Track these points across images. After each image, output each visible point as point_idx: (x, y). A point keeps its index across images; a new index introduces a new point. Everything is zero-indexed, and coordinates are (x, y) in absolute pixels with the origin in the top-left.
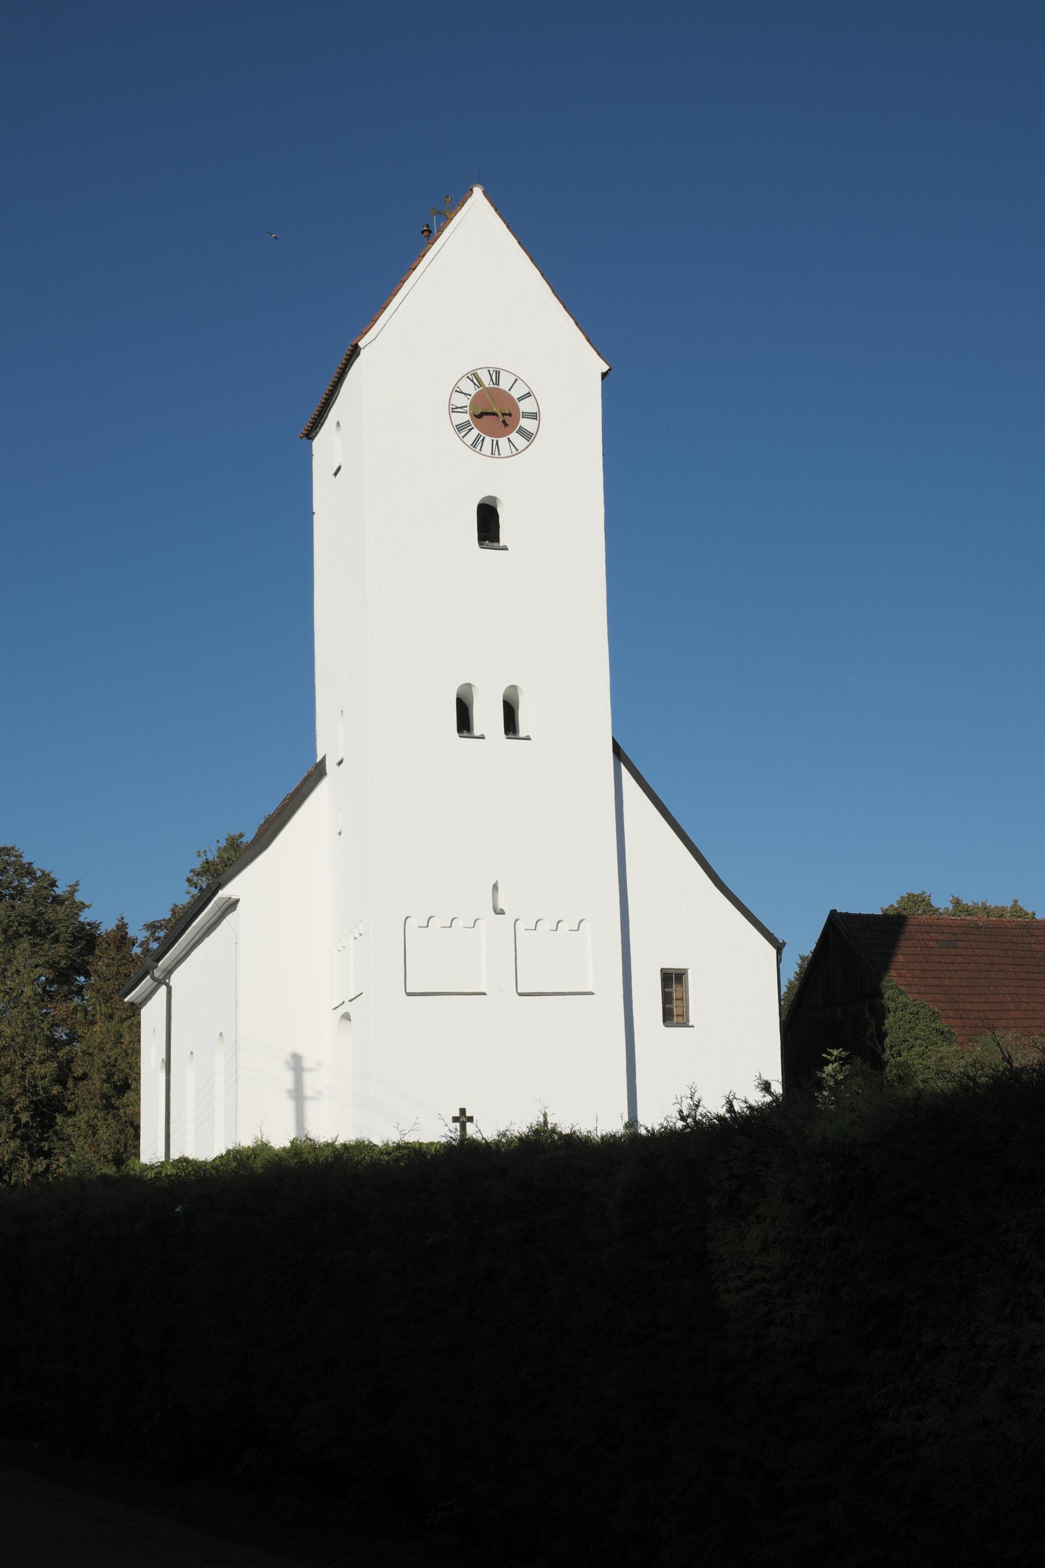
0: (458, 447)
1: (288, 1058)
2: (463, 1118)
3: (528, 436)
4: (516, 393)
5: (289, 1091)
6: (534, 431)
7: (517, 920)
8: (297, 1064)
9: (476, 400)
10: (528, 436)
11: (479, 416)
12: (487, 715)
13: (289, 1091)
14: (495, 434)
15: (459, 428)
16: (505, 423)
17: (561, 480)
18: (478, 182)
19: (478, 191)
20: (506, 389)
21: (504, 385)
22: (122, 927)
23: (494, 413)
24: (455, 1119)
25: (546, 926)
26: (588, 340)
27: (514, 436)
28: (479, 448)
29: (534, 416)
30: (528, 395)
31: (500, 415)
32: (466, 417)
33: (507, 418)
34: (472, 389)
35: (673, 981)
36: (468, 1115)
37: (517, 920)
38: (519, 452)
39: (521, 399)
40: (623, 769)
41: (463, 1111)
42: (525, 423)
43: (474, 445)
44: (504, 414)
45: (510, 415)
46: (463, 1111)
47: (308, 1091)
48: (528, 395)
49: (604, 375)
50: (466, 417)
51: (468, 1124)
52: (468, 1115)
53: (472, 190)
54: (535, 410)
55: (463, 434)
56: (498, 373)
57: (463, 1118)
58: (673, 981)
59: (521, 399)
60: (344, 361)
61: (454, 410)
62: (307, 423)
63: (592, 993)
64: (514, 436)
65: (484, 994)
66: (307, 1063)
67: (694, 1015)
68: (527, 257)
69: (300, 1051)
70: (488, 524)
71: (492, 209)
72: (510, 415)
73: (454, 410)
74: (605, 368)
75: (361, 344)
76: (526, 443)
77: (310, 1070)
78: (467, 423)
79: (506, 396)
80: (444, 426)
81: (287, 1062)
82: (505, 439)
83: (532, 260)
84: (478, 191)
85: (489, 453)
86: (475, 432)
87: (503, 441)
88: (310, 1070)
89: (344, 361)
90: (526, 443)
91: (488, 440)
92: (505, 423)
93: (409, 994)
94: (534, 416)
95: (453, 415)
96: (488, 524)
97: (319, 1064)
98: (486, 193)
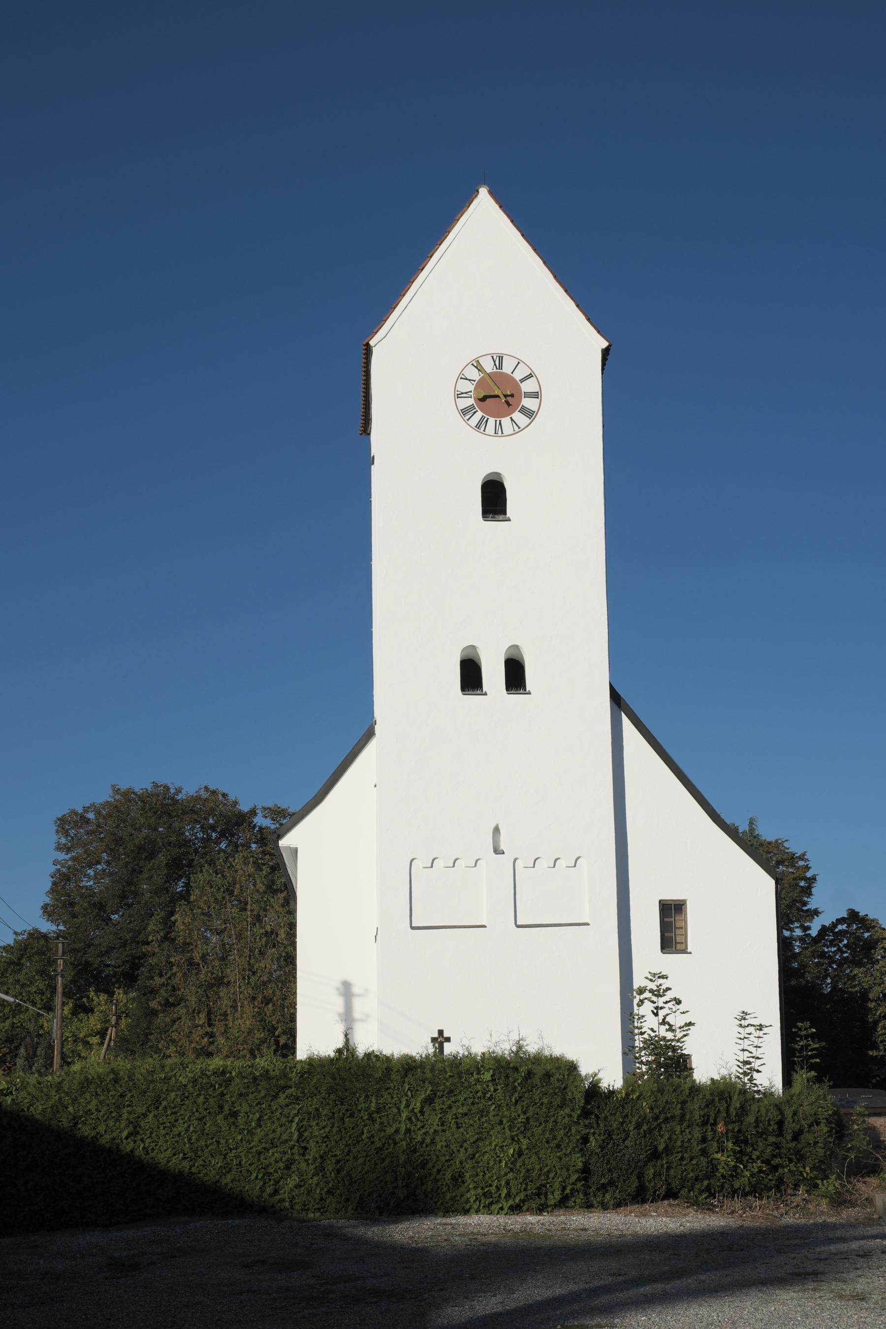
0: (464, 430)
1: (339, 985)
2: (440, 1039)
3: (530, 414)
4: (518, 376)
5: (340, 1015)
6: (535, 409)
7: (515, 860)
8: (347, 991)
9: (480, 384)
10: (530, 414)
11: (483, 399)
12: (493, 674)
13: (340, 1015)
14: (498, 414)
15: (464, 412)
16: (508, 404)
17: (563, 455)
18: (484, 183)
19: (483, 192)
20: (509, 372)
21: (507, 369)
22: (816, 912)
23: (498, 396)
24: (434, 1040)
25: (543, 864)
26: (589, 320)
27: (517, 416)
28: (483, 428)
29: (536, 395)
30: (530, 376)
31: (502, 396)
32: (471, 401)
33: (509, 399)
34: (476, 375)
35: (671, 913)
36: (445, 1035)
37: (515, 860)
38: (521, 430)
39: (522, 380)
40: (626, 721)
41: (441, 1032)
42: (526, 402)
43: (478, 426)
44: (506, 396)
45: (512, 396)
46: (441, 1032)
47: (357, 1014)
48: (530, 376)
49: (606, 353)
50: (471, 401)
51: (445, 1044)
52: (445, 1035)
53: (478, 191)
54: (537, 390)
55: (468, 417)
56: (501, 358)
57: (440, 1039)
58: (671, 913)
59: (522, 380)
60: (364, 361)
61: (459, 395)
62: (359, 428)
63: (588, 924)
64: (517, 416)
65: (485, 926)
66: (356, 990)
67: (485, 689)
68: (530, 248)
69: (349, 979)
70: (494, 500)
71: (497, 207)
72: (512, 396)
73: (459, 395)
74: (605, 344)
75: (372, 343)
76: (461, 407)
77: (359, 995)
78: (472, 407)
79: (509, 379)
80: (449, 410)
81: (338, 989)
82: (508, 418)
83: (535, 250)
84: (483, 192)
85: (493, 433)
86: (479, 414)
87: (506, 421)
88: (359, 995)
89: (364, 361)
90: (529, 421)
91: (492, 421)
92: (508, 404)
93: (413, 928)
94: (536, 395)
95: (458, 400)
96: (494, 500)
97: (367, 990)
98: (491, 193)
